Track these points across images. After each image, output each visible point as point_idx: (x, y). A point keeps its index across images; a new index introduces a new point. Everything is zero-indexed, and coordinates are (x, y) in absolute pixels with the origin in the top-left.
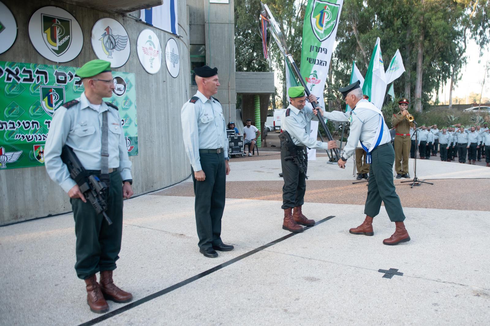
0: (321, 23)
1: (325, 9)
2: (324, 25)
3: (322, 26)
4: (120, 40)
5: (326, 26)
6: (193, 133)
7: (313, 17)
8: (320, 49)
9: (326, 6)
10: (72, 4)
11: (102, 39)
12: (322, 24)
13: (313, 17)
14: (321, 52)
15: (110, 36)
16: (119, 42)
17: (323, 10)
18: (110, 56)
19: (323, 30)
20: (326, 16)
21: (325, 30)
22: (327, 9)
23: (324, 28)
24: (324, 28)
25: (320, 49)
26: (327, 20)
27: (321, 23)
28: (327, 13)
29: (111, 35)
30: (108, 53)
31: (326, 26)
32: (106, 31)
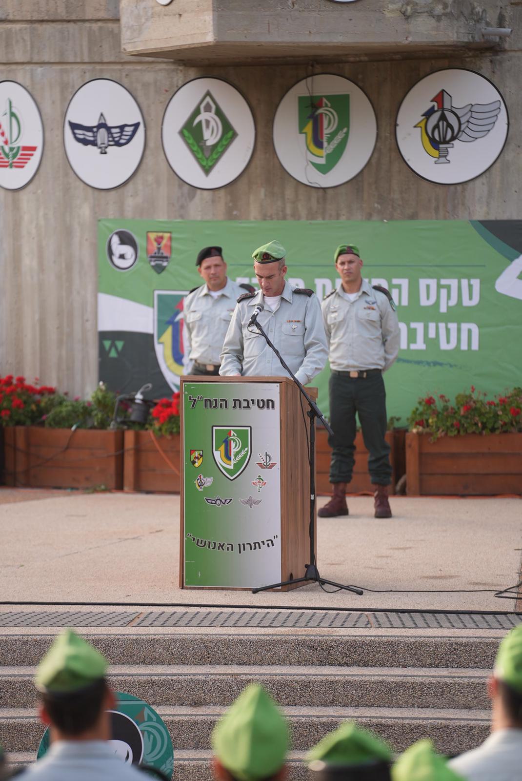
0: (228, 456)
1: (230, 436)
2: (233, 457)
3: (229, 458)
4: (474, 115)
5: (235, 458)
6: (263, 46)
7: (216, 450)
8: (257, 545)
9: (231, 432)
10: (360, 61)
11: (423, 125)
12: (229, 456)
13: (216, 450)
14: (260, 548)
15: (446, 113)
16: (472, 120)
17: (227, 438)
18: (443, 160)
19: (232, 465)
20: (233, 445)
21: (234, 464)
22: (232, 435)
23: (233, 462)
24: (233, 462)
25: (257, 545)
26: (236, 450)
27: (228, 456)
28: (234, 441)
29: (447, 110)
30: (436, 153)
31: (235, 458)
32: (435, 104)
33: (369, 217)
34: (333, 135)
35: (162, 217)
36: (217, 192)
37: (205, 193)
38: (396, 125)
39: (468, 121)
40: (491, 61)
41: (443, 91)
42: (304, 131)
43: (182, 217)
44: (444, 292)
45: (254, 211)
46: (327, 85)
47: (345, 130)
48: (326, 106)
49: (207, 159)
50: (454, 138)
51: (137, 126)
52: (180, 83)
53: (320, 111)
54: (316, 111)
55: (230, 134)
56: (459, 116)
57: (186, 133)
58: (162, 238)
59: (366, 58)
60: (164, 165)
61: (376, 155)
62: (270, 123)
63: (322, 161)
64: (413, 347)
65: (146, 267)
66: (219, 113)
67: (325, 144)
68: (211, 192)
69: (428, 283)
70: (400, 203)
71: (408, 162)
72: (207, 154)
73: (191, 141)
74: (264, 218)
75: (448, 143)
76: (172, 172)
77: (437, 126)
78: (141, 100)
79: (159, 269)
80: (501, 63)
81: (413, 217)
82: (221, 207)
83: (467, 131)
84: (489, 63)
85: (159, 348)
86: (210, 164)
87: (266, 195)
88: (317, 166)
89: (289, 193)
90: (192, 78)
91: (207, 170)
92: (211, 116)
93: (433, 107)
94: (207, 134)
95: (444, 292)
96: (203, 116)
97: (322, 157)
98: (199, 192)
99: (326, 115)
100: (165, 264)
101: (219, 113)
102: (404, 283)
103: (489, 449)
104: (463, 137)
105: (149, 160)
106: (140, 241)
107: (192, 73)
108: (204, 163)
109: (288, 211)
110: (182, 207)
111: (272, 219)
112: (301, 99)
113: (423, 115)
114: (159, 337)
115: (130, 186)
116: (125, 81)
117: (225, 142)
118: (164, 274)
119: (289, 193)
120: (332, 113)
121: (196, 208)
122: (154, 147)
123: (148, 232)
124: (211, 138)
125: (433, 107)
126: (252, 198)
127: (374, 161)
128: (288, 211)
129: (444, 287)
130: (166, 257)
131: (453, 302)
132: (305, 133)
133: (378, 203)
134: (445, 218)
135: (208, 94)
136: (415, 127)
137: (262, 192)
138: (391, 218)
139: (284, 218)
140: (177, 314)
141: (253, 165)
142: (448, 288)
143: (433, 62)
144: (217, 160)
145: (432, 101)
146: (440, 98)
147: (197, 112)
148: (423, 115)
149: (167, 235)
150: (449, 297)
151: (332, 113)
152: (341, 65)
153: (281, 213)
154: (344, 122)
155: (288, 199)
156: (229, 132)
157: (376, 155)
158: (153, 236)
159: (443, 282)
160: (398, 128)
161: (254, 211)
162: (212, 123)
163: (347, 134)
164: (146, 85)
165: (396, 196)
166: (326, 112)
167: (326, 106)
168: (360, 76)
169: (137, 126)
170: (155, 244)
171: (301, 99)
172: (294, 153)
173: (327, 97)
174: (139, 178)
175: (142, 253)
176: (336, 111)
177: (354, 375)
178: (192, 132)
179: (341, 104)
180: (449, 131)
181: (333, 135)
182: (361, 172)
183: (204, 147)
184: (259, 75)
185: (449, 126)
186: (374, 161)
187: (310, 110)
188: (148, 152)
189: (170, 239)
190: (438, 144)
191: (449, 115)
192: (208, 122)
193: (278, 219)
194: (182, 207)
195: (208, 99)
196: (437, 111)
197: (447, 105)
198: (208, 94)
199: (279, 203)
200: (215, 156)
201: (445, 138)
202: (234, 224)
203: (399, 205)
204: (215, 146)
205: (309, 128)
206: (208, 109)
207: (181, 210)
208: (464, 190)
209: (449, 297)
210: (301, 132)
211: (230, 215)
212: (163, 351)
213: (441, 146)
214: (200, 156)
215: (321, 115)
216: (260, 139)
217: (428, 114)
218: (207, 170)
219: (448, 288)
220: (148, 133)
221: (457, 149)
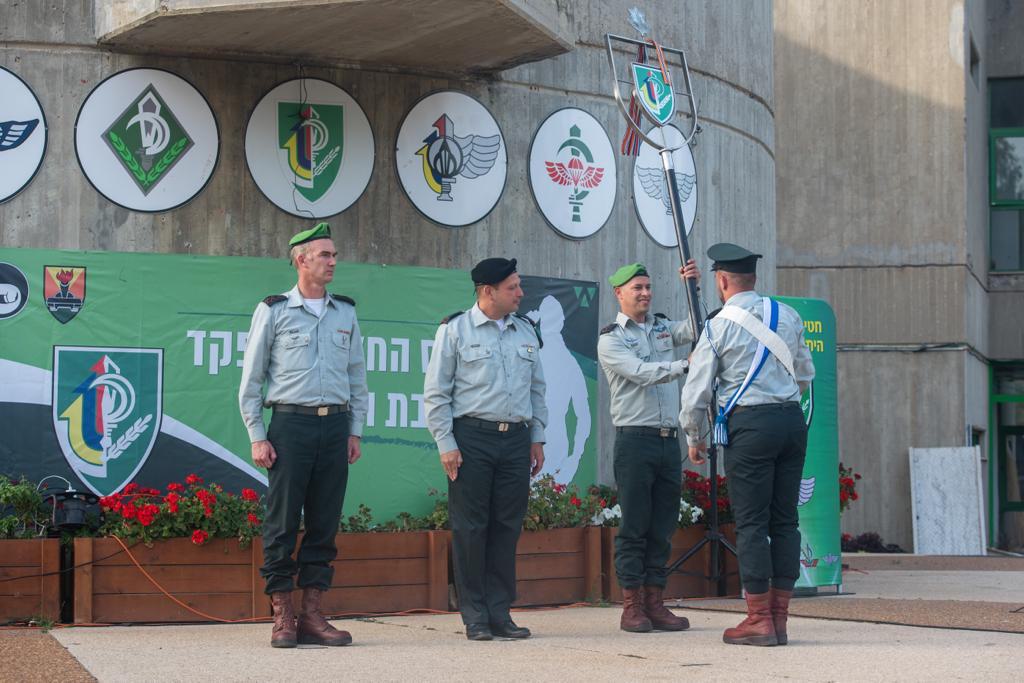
10: (352, 69)
11: (424, 151)
16: (473, 153)
18: (445, 196)
30: (438, 187)
32: (436, 128)
33: (365, 259)
34: (322, 154)
35: (71, 244)
36: (159, 217)
37: (142, 216)
38: (395, 149)
39: (470, 154)
40: (489, 90)
41: (445, 115)
42: (286, 145)
43: (103, 246)
44: (214, 348)
45: (214, 243)
46: (320, 93)
47: (337, 149)
48: (314, 117)
49: (147, 173)
50: (456, 172)
51: (32, 125)
52: (106, 73)
53: (307, 123)
54: (302, 122)
55: (182, 143)
56: (462, 147)
57: (114, 137)
58: (70, 274)
59: (358, 67)
60: (77, 176)
61: (373, 183)
62: (241, 132)
63: (310, 185)
64: (414, 424)
65: (38, 312)
66: (166, 113)
67: (313, 164)
68: (151, 216)
69: (377, 342)
70: (400, 244)
71: (410, 196)
72: (147, 165)
73: (122, 148)
74: (230, 253)
75: (450, 176)
76: (89, 187)
77: (438, 156)
78: (41, 90)
79: (64, 317)
80: (498, 93)
81: (414, 262)
82: (166, 235)
83: (469, 165)
84: (487, 92)
85: (60, 427)
86: (151, 178)
87: (232, 224)
88: (304, 191)
89: (265, 223)
90: (125, 68)
91: (146, 188)
92: (153, 117)
93: (436, 132)
94: (147, 140)
95: (214, 348)
96: (142, 117)
97: (309, 180)
98: (131, 214)
99: (314, 128)
100: (75, 310)
101: (166, 113)
102: (405, 343)
103: (539, 548)
104: (466, 172)
105: (52, 170)
106: (33, 279)
107: (125, 61)
108: (142, 177)
109: (264, 245)
110: (105, 233)
111: (241, 255)
112: (282, 106)
113: (424, 141)
114: (59, 413)
115: (17, 203)
116: (16, 67)
117: (174, 152)
118: (71, 323)
119: (265, 223)
120: (322, 128)
121: (125, 236)
122: (61, 150)
123: (45, 266)
124: (152, 145)
125: (436, 132)
126: (211, 226)
127: (370, 190)
128: (264, 245)
129: (215, 340)
130: (79, 301)
131: (226, 360)
132: (288, 148)
133: (375, 242)
134: (447, 266)
135: (151, 89)
136: (416, 154)
137: (228, 218)
138: (390, 263)
139: (258, 253)
140: (93, 378)
141: (214, 182)
142: (220, 341)
143: (434, 80)
144: (162, 175)
145: (434, 125)
146: (441, 122)
147: (132, 110)
148: (424, 141)
149: (78, 272)
150: (220, 356)
151: (322, 128)
152: (332, 70)
153: (254, 247)
154: (337, 139)
155: (264, 230)
156: (180, 140)
157: (373, 183)
158: (53, 272)
159: (395, 341)
160: (398, 152)
161: (214, 243)
162: (156, 126)
163: (340, 153)
164: (51, 73)
165: (396, 235)
166: (315, 125)
167: (314, 117)
168: (354, 86)
169: (32, 125)
170: (58, 283)
171: (282, 106)
172: (273, 170)
173: (318, 107)
174: (33, 194)
175: (35, 295)
176: (326, 125)
177: (850, 539)
178: (123, 136)
179: (333, 117)
180: (452, 164)
181: (322, 154)
182: (356, 202)
183: (142, 156)
184: (227, 68)
185: (451, 157)
186: (370, 190)
187: (294, 122)
188: (49, 159)
189: (85, 275)
190: (442, 175)
191: (451, 144)
192: (149, 125)
193: (250, 255)
194: (105, 233)
195: (150, 95)
196: (439, 138)
197: (449, 133)
198: (151, 89)
199: (252, 235)
200: (158, 169)
201: (447, 171)
202: (187, 259)
203: (399, 247)
204: (158, 157)
205: (292, 142)
206: (149, 107)
207: (104, 240)
208: (466, 235)
209: (220, 356)
210: (282, 147)
211: (179, 246)
212: (68, 429)
213: (444, 180)
214: (135, 167)
215: (308, 127)
216: (224, 153)
217: (431, 140)
218: (146, 188)
219: (220, 341)
220: (50, 133)
221: (461, 185)
